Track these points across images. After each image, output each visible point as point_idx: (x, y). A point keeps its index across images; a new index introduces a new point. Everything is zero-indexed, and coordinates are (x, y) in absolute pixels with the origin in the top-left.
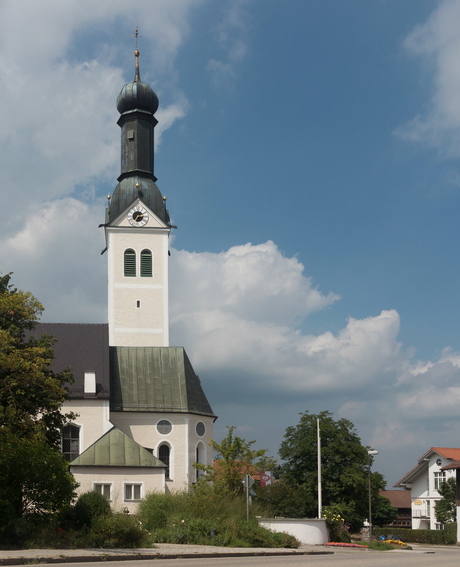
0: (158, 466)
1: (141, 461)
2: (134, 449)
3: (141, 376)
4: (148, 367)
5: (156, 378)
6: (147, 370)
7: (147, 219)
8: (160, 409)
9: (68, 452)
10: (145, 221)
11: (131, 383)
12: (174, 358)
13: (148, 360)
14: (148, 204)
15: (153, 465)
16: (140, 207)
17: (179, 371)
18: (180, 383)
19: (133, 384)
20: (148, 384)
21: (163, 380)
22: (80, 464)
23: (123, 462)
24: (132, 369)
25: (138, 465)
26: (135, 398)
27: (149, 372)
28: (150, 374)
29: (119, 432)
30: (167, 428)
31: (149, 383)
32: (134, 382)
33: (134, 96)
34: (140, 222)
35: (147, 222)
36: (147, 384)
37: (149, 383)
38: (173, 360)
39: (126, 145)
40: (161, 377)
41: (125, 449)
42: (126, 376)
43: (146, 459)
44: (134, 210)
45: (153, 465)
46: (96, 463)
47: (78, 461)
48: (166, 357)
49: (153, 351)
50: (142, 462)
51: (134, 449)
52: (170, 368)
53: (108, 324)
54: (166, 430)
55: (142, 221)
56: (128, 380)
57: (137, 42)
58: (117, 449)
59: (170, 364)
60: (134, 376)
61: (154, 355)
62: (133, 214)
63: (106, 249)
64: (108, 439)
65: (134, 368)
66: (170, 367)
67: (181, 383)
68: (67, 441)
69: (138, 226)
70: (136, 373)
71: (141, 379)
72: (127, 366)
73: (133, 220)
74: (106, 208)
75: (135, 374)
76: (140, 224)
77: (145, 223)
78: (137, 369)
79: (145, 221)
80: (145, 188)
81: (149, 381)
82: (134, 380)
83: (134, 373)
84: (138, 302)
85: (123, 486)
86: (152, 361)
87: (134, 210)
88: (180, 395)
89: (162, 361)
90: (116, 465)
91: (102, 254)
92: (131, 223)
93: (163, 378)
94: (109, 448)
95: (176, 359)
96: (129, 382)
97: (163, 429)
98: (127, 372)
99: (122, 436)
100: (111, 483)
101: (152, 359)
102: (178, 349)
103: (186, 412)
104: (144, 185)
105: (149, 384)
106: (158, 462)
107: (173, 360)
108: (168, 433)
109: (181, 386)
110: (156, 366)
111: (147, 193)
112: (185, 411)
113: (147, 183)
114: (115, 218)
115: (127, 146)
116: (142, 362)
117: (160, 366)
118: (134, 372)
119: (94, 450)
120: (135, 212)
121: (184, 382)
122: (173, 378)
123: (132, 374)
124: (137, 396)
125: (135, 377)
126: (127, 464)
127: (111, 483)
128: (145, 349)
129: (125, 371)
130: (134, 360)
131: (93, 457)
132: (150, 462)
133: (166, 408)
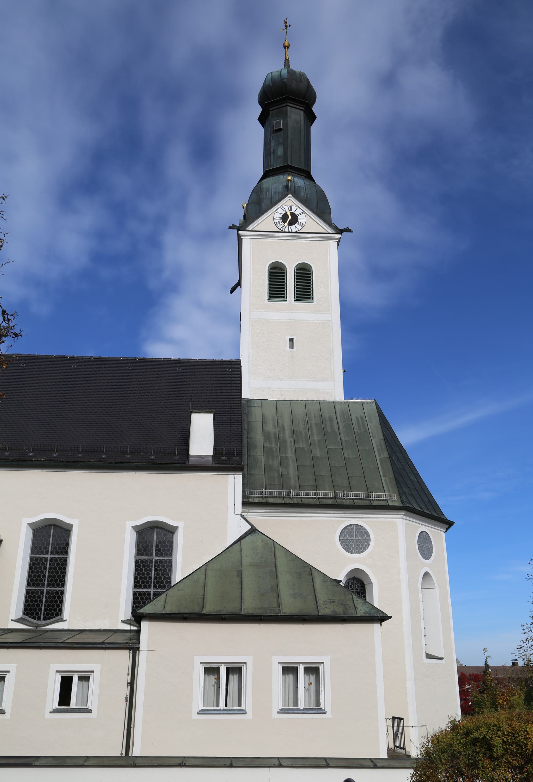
0: (364, 615)
1: (320, 602)
2: (300, 574)
3: (302, 445)
4: (314, 430)
5: (331, 448)
6: (312, 435)
7: (303, 222)
8: (344, 500)
9: (145, 587)
10: (301, 224)
11: (284, 455)
12: (361, 417)
13: (313, 419)
14: (305, 202)
15: (351, 612)
16: (293, 206)
17: (373, 436)
18: (377, 456)
19: (287, 458)
20: (317, 457)
21: (345, 451)
22: (168, 610)
23: (275, 605)
24: (284, 434)
25: (315, 613)
26: (293, 481)
27: (316, 438)
28: (319, 441)
29: (262, 541)
30: (360, 542)
31: (319, 455)
32: (290, 454)
33: (284, 80)
34: (294, 226)
35: (303, 226)
36: (313, 458)
37: (319, 456)
38: (360, 420)
39: (271, 139)
40: (340, 447)
41: (279, 575)
42: (273, 443)
43: (331, 598)
44: (284, 209)
45: (352, 613)
46: (208, 609)
47: (162, 603)
48: (347, 417)
49: (321, 407)
50: (322, 606)
51: (300, 574)
52: (356, 432)
53: (240, 361)
54: (359, 545)
55: (296, 225)
56: (277, 452)
57: (286, 36)
58: (260, 576)
59: (356, 427)
60: (289, 444)
61: (323, 412)
62: (282, 215)
63: (239, 284)
64: (239, 553)
65: (288, 432)
66: (356, 431)
67: (380, 456)
68: (145, 563)
69: (291, 231)
70: (292, 440)
71: (303, 449)
72: (275, 428)
73: (283, 223)
74: (240, 220)
75: (291, 441)
76: (294, 228)
77: (300, 227)
78: (294, 434)
79: (301, 224)
80: (300, 185)
81: (318, 453)
82: (289, 451)
83: (289, 440)
84: (291, 340)
85: (93, 670)
86: (320, 421)
87: (284, 209)
88: (382, 475)
89: (339, 421)
90: (258, 612)
91: (231, 292)
92: (280, 228)
93: (344, 448)
94: (240, 574)
95: (364, 418)
96: (279, 454)
97: (353, 542)
98: (275, 437)
99: (271, 548)
100: (391, 616)
101: (320, 419)
102: (367, 403)
103: (398, 505)
104: (299, 183)
105: (318, 458)
106: (361, 605)
107: (360, 420)
108: (362, 552)
109: (381, 460)
110: (329, 429)
111: (303, 191)
112: (396, 504)
113: (303, 181)
114: (255, 220)
115: (273, 139)
116: (303, 423)
117: (336, 428)
118: (289, 437)
119: (203, 577)
120: (285, 212)
121: (386, 455)
122: (364, 448)
123: (285, 441)
124: (297, 477)
125: (291, 446)
126: (286, 610)
127: (391, 616)
128: (306, 403)
129: (272, 436)
130: (287, 423)
131: (202, 593)
132: (342, 604)
133: (357, 499)
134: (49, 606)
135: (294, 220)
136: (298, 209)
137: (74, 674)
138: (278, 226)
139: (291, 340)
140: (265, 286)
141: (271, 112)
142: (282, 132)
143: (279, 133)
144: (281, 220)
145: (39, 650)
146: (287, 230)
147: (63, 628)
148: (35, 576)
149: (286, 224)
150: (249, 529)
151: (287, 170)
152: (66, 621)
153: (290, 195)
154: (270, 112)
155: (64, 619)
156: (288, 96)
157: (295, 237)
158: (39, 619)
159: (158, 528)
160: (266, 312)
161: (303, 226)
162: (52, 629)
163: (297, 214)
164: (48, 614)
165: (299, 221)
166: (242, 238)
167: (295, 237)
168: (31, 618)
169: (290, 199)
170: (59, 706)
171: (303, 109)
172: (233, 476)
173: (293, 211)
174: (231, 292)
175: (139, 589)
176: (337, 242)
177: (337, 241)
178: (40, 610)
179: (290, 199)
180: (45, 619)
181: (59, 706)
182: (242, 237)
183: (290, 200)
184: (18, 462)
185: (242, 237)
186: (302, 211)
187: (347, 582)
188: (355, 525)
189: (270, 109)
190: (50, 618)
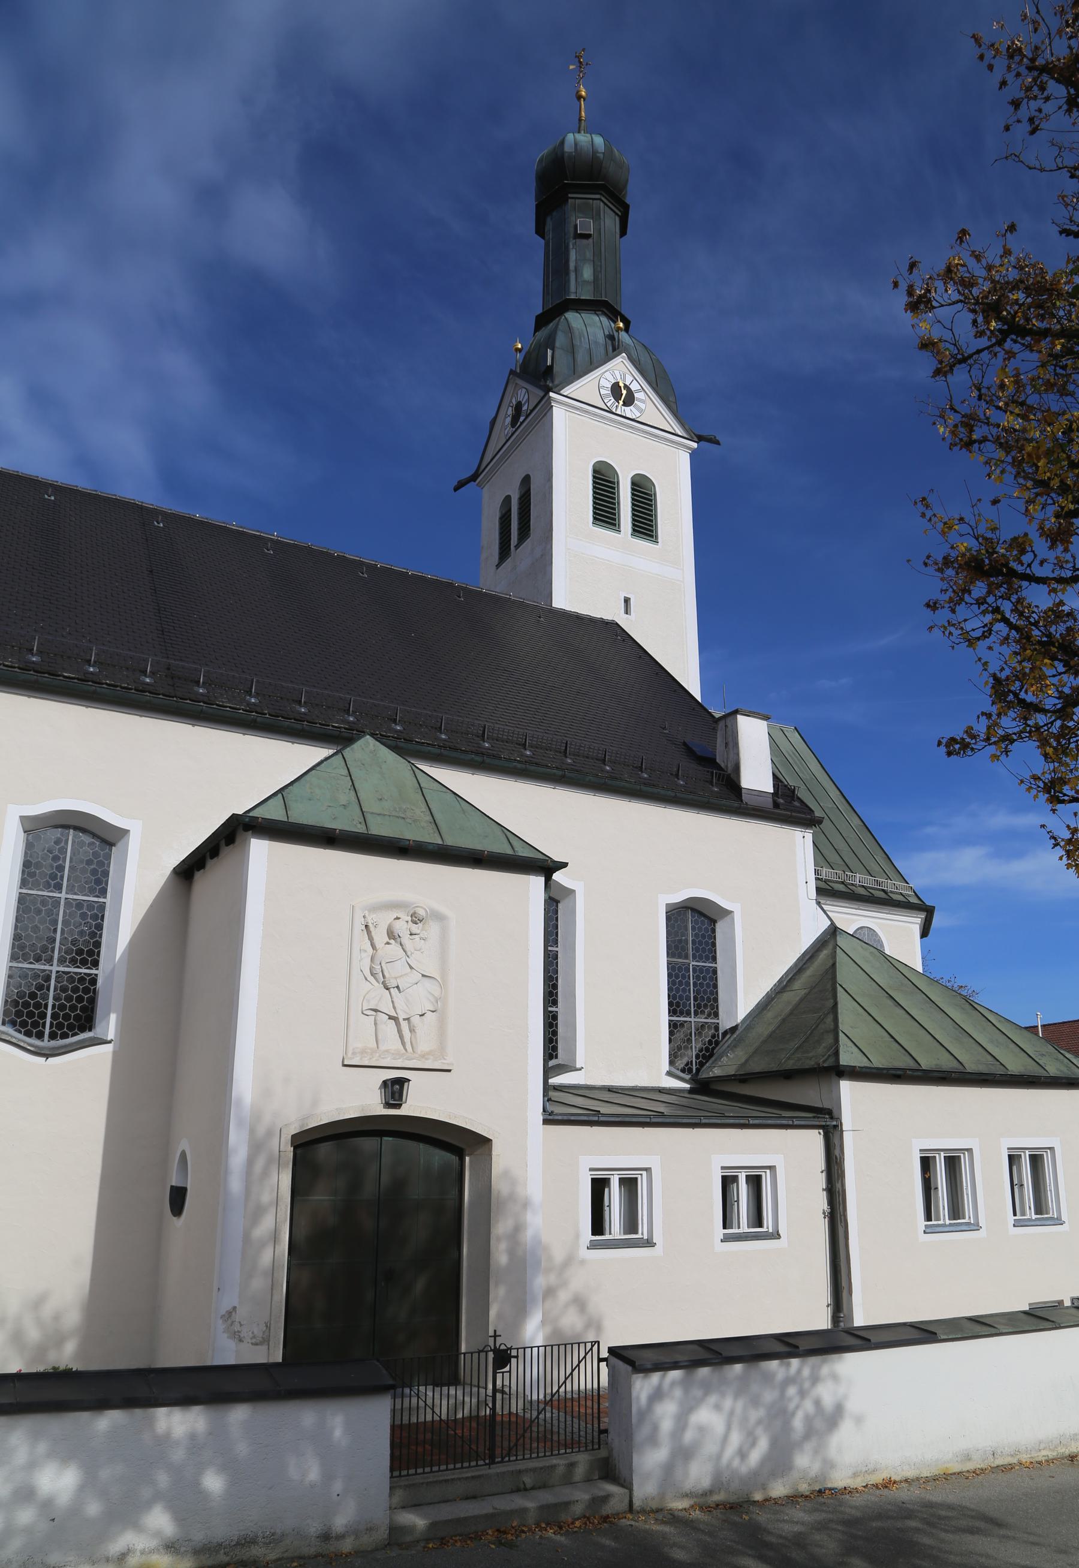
7: (642, 406)
33: (598, 155)
55: (632, 407)
76: (629, 411)
84: (627, 601)
91: (456, 489)
134: (62, 1007)
135: (629, 401)
136: (635, 381)
137: (613, 1175)
138: (606, 401)
139: (627, 601)
140: (588, 498)
141: (570, 200)
142: (591, 240)
143: (584, 241)
144: (610, 392)
145: (589, 1127)
146: (619, 412)
147: (577, 1083)
148: (677, 990)
149: (621, 402)
150: (828, 925)
151: (602, 309)
152: (580, 1069)
153: (624, 354)
154: (568, 200)
155: (578, 1066)
156: (608, 185)
157: (632, 427)
158: (40, 1036)
159: (693, 910)
160: (590, 543)
161: (641, 411)
162: (561, 1084)
163: (633, 390)
164: (60, 1026)
165: (636, 402)
166: (552, 406)
167: (632, 427)
168: (20, 1032)
169: (623, 360)
170: (592, 1235)
171: (620, 214)
172: (801, 834)
173: (628, 384)
174: (456, 489)
175: (679, 1017)
176: (689, 454)
177: (690, 452)
178: (43, 1016)
179: (623, 360)
180: (53, 1036)
181: (592, 1235)
182: (552, 404)
183: (623, 363)
184: (442, 750)
185: (552, 404)
186: (640, 388)
187: (47, 972)
188: (867, 927)
189: (570, 195)
190: (65, 1036)
